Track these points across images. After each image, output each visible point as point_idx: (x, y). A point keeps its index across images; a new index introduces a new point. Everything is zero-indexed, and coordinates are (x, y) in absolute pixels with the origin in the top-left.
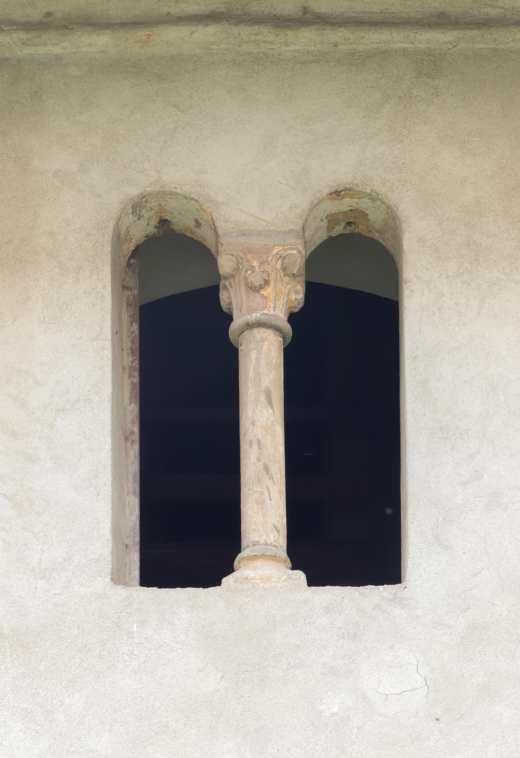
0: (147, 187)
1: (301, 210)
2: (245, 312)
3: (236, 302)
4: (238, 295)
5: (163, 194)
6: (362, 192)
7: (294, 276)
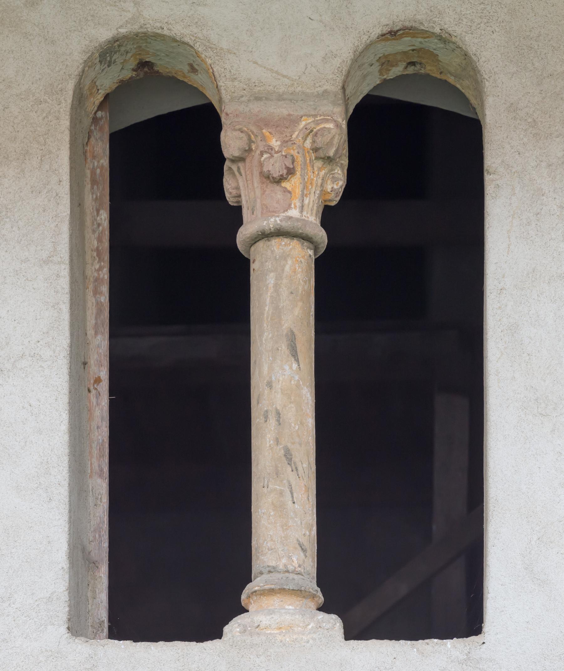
0: (121, 27)
1: (340, 61)
2: (259, 216)
3: (247, 197)
4: (250, 186)
5: (143, 38)
6: (427, 31)
7: (329, 160)
